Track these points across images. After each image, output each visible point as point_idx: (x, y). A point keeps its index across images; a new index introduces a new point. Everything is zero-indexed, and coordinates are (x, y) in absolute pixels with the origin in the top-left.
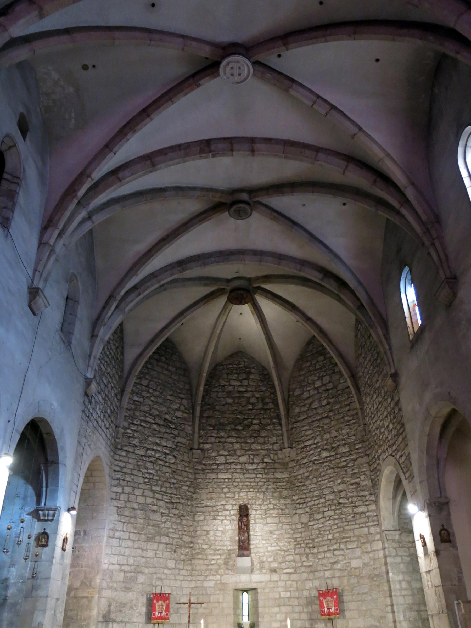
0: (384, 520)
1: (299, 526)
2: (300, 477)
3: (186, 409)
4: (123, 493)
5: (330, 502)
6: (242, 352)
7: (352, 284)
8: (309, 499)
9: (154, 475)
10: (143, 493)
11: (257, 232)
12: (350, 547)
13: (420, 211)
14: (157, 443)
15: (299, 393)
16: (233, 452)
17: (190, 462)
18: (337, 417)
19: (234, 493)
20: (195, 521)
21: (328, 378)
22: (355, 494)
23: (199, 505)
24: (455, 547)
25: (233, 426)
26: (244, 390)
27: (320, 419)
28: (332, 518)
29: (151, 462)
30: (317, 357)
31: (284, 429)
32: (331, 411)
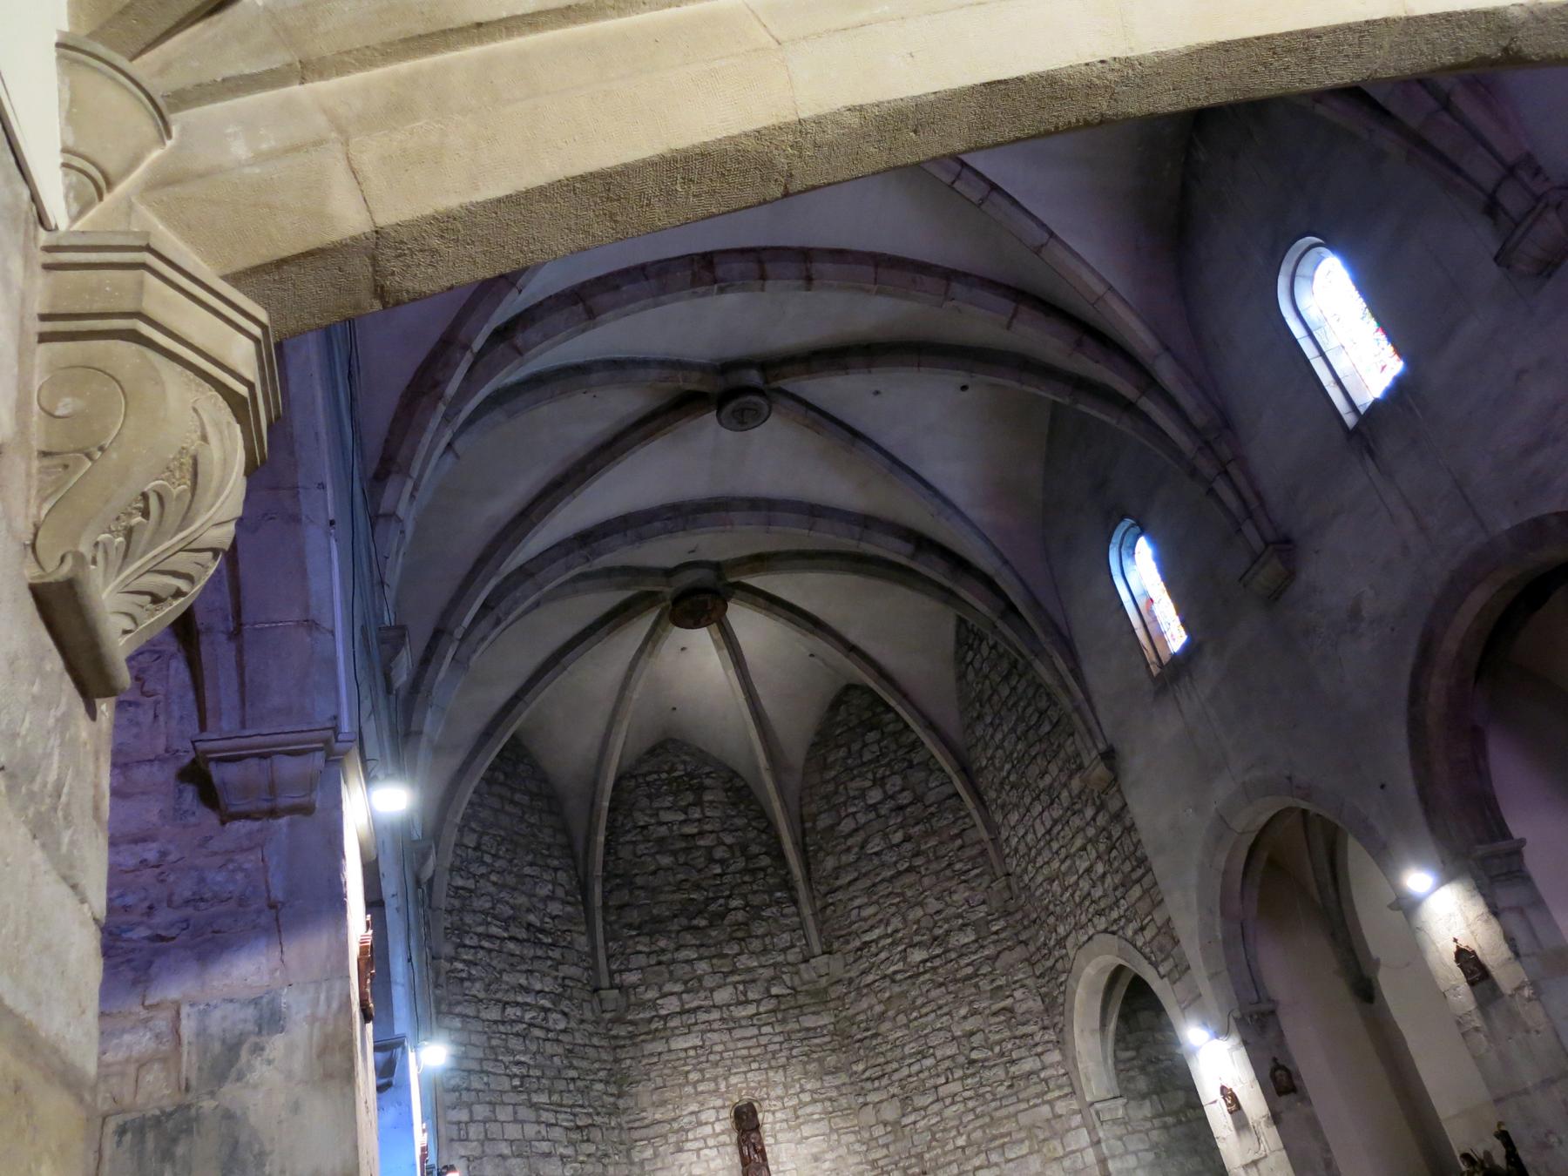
0: (1088, 1080)
1: (879, 1131)
2: (862, 1017)
3: (567, 893)
4: (472, 1121)
5: (947, 1063)
6: (674, 741)
7: (984, 561)
8: (895, 1065)
9: (529, 1066)
10: (515, 1113)
11: (770, 459)
12: (1013, 1156)
13: (1187, 401)
14: (521, 986)
15: (829, 822)
16: (694, 983)
17: (597, 1023)
18: (934, 866)
19: (715, 1079)
20: (632, 1163)
21: (897, 780)
22: (1007, 1034)
23: (637, 1124)
24: (1305, 1099)
25: (684, 922)
26: (695, 831)
27: (893, 877)
28: (958, 1099)
29: (517, 1035)
30: (863, 735)
31: (807, 911)
32: (917, 854)
